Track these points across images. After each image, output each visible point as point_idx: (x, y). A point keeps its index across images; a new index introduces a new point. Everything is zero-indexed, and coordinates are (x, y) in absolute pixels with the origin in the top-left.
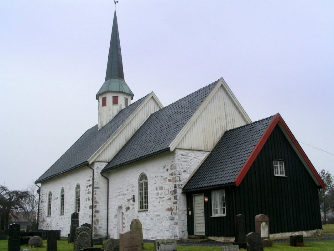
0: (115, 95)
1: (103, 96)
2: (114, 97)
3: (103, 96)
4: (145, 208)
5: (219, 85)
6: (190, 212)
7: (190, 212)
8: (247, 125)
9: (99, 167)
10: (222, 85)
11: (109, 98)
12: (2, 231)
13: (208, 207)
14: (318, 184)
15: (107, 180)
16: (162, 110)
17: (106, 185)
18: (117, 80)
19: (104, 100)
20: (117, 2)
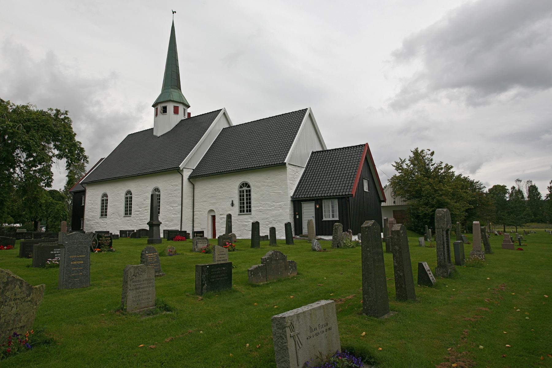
0: (176, 105)
1: (164, 105)
2: (174, 106)
3: (164, 105)
4: (247, 212)
5: (221, 113)
6: (297, 217)
7: (297, 217)
8: (323, 151)
9: (187, 174)
10: (224, 113)
11: (170, 107)
12: (162, 236)
13: (319, 213)
14: (382, 199)
15: (192, 186)
16: (231, 127)
17: (191, 190)
18: (177, 91)
19: (165, 110)
20: (175, 12)
